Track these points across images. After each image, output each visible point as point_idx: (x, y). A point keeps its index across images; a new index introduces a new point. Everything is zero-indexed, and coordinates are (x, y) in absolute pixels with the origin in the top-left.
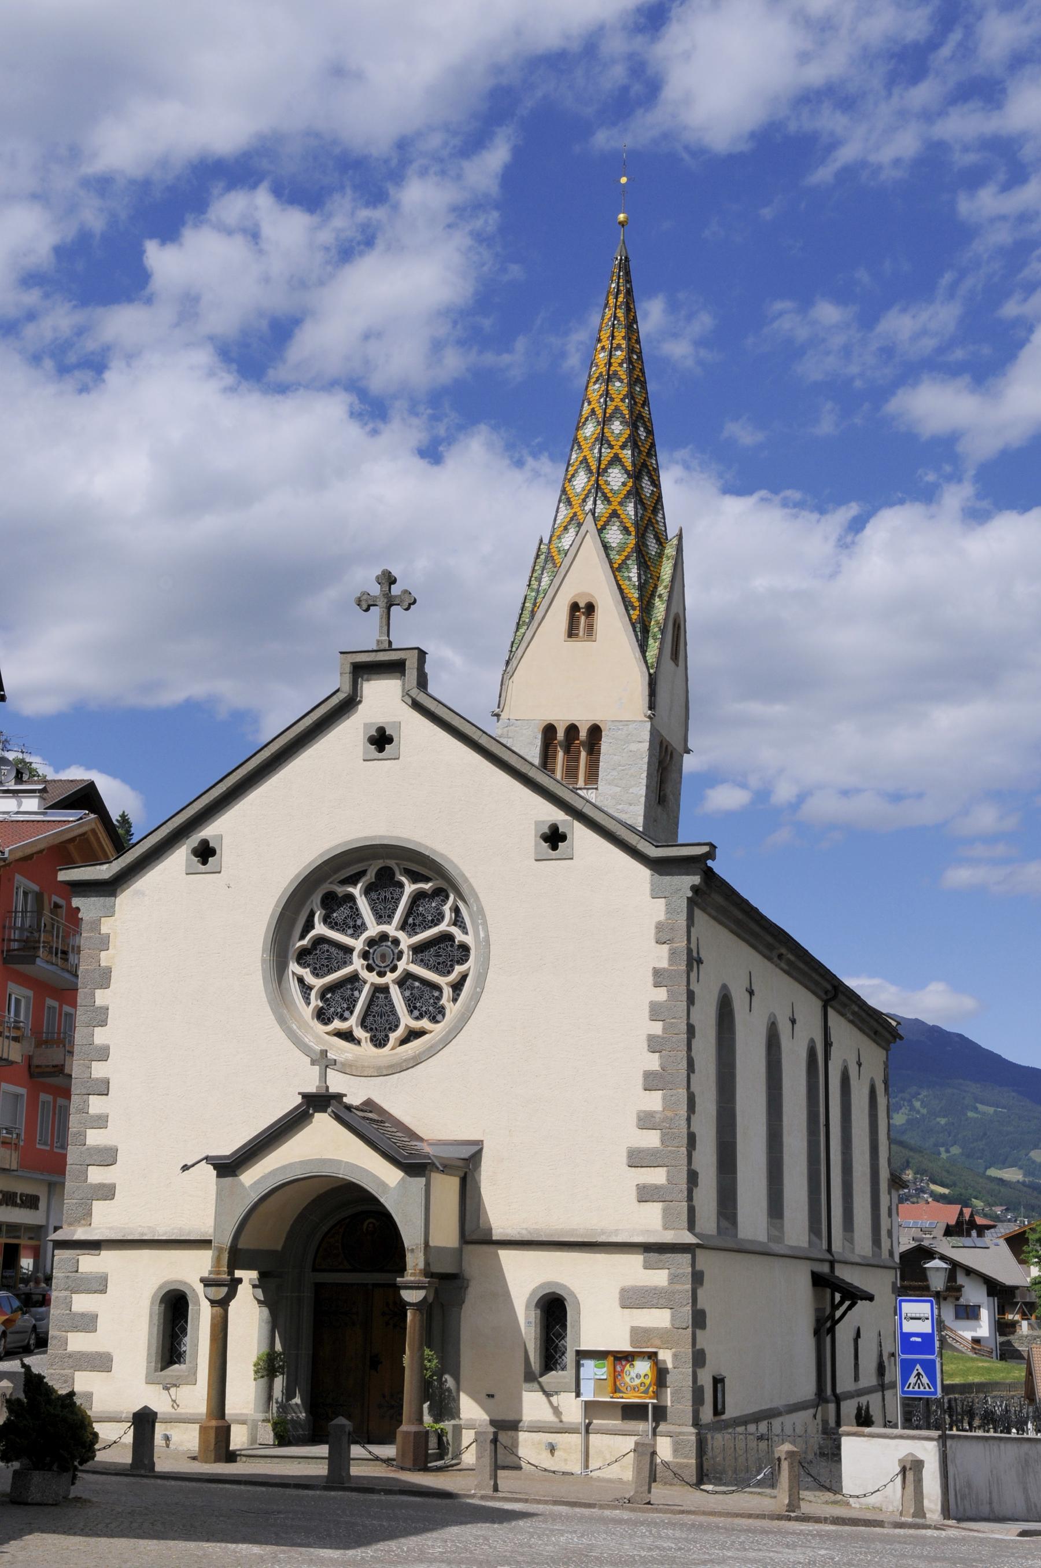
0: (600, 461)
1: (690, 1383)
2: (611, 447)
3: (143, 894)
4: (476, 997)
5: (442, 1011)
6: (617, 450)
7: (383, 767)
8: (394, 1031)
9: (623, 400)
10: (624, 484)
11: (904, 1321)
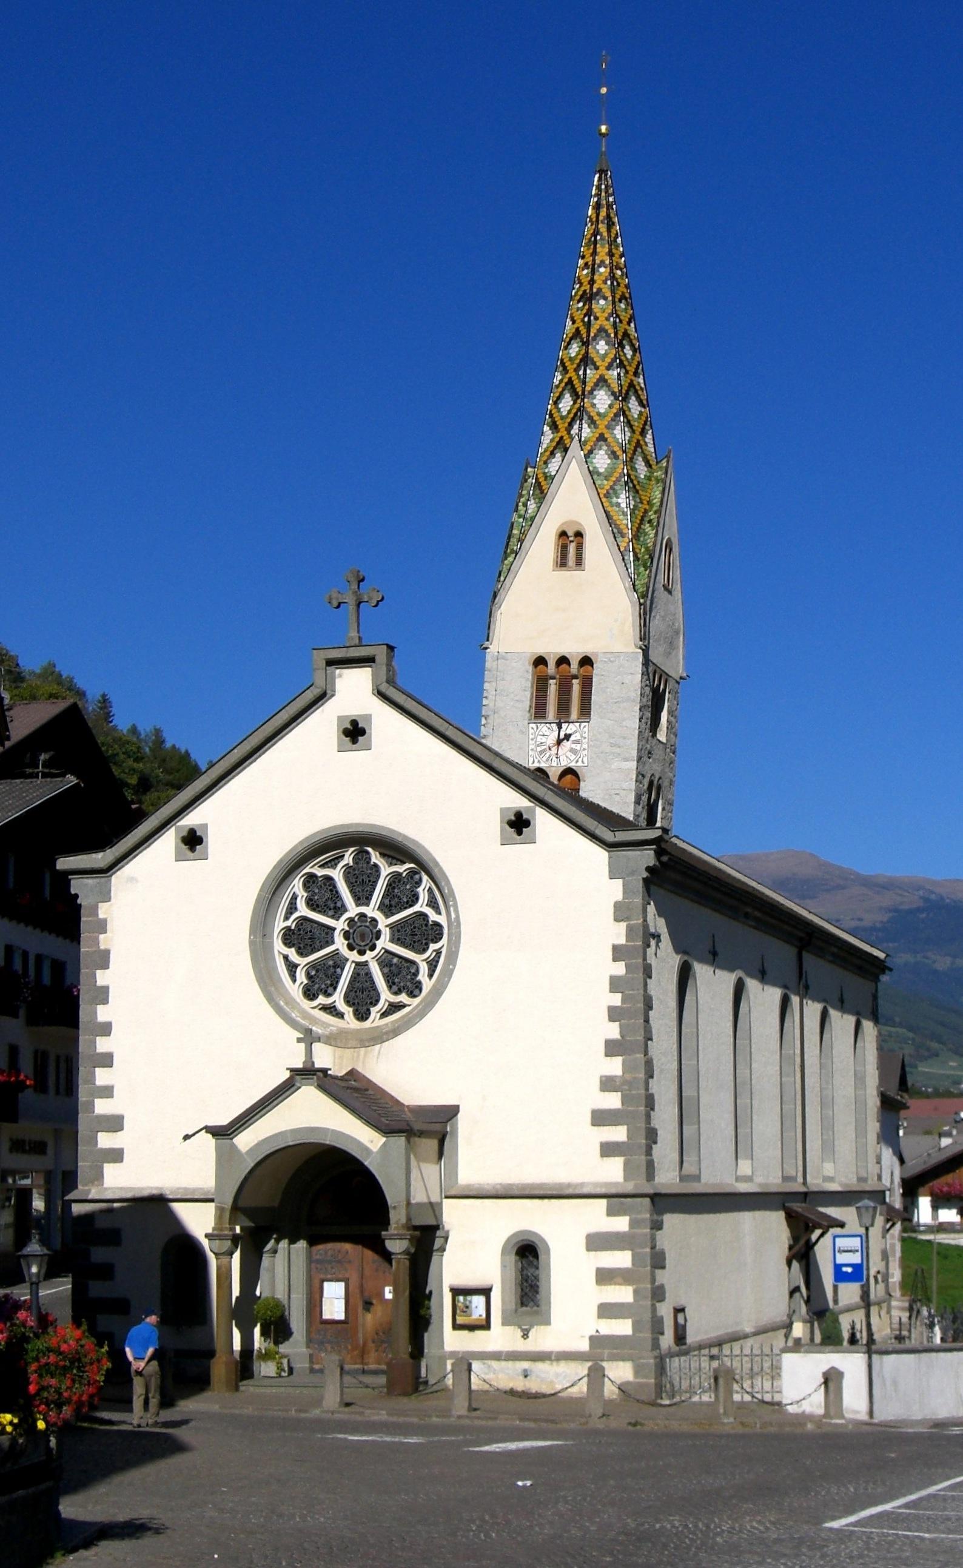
0: (584, 383)
1: (650, 1315)
2: (597, 368)
3: (137, 881)
4: (448, 974)
5: (419, 986)
6: (602, 370)
7: (356, 757)
9: (607, 319)
10: (610, 406)
11: (837, 1254)
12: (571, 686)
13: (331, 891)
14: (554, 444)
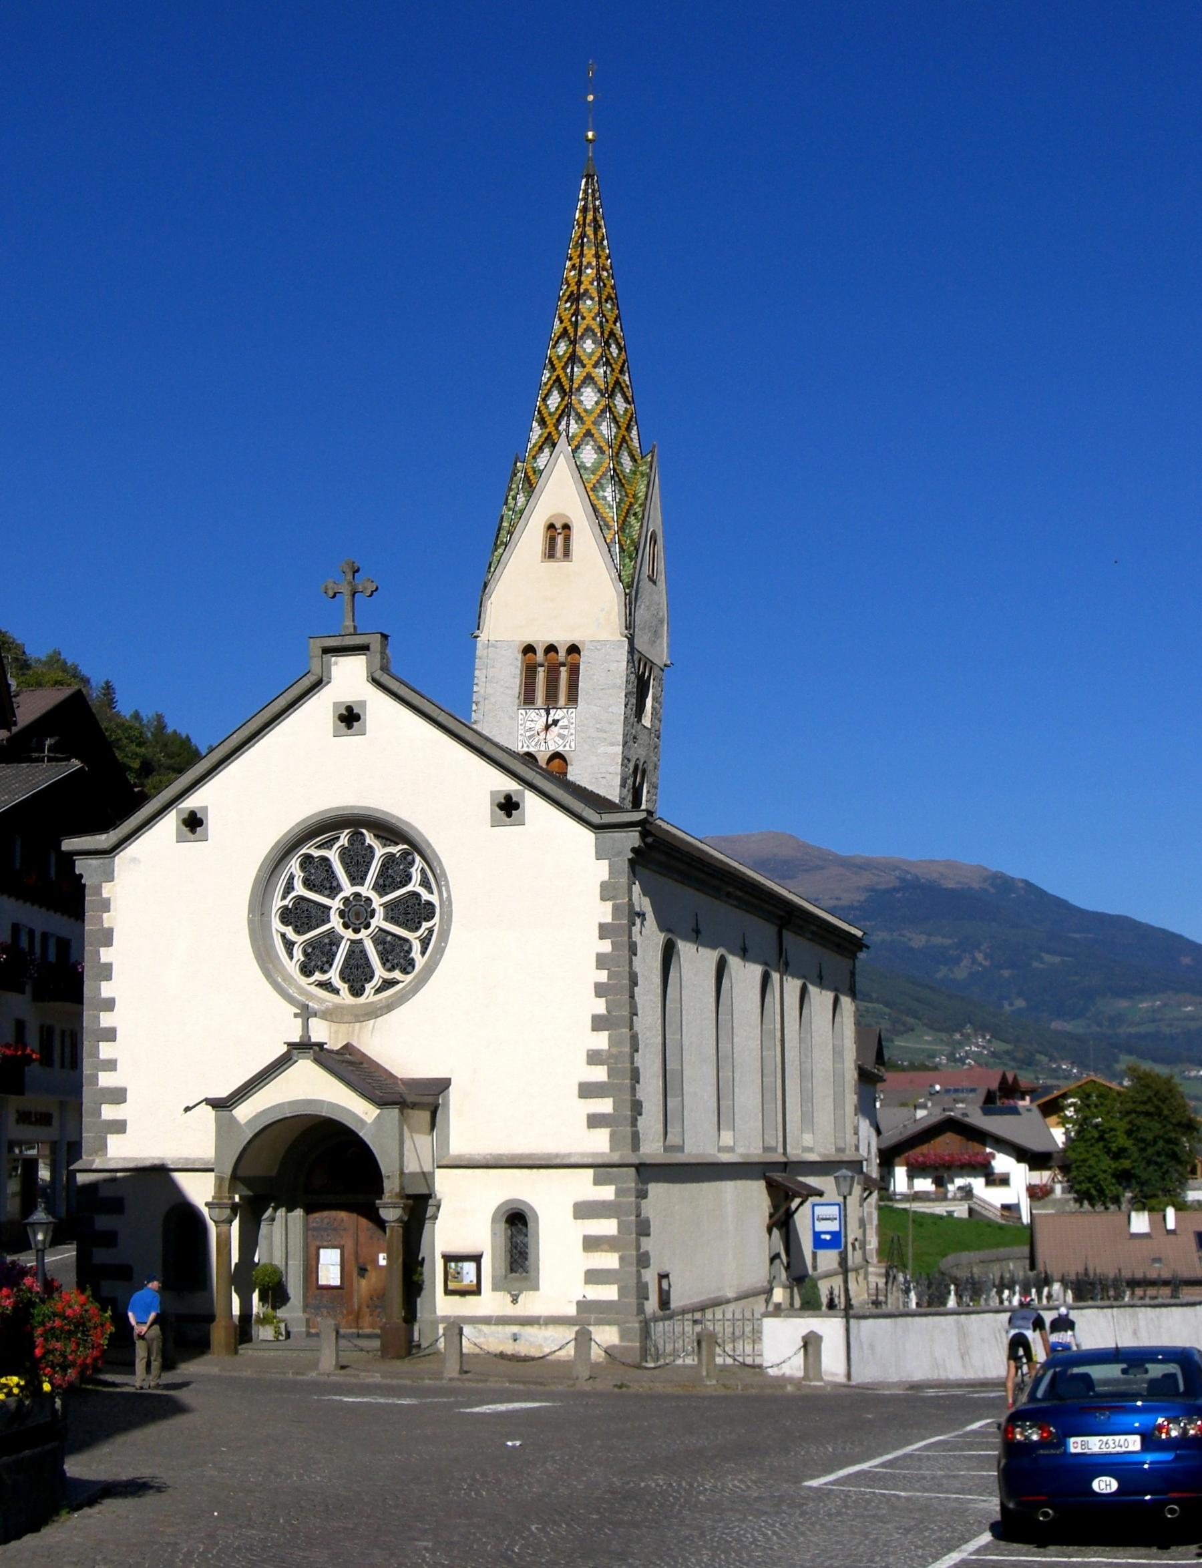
0: (572, 380)
2: (584, 366)
3: (140, 862)
4: (440, 951)
5: (412, 963)
6: (589, 368)
7: (351, 742)
9: (594, 319)
10: (597, 403)
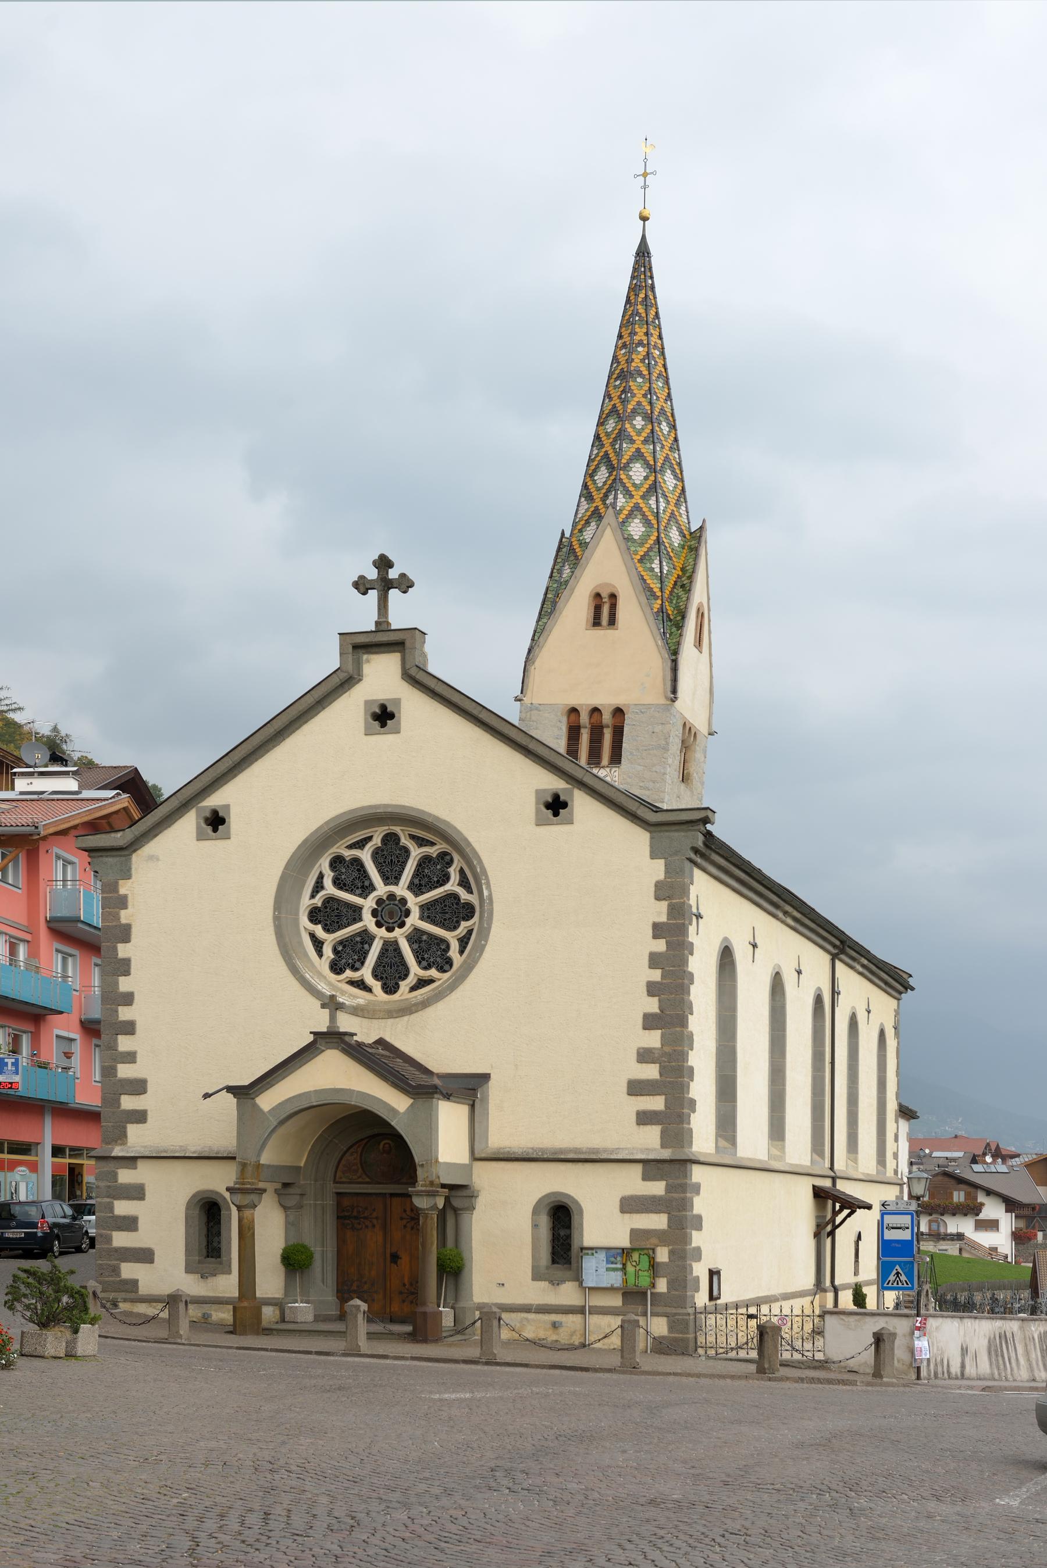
3: (158, 860)
5: (449, 962)
6: (638, 444)
7: (384, 741)
8: (404, 979)
10: (646, 478)
11: (886, 1231)
12: (602, 734)
13: (358, 870)
14: (589, 513)
